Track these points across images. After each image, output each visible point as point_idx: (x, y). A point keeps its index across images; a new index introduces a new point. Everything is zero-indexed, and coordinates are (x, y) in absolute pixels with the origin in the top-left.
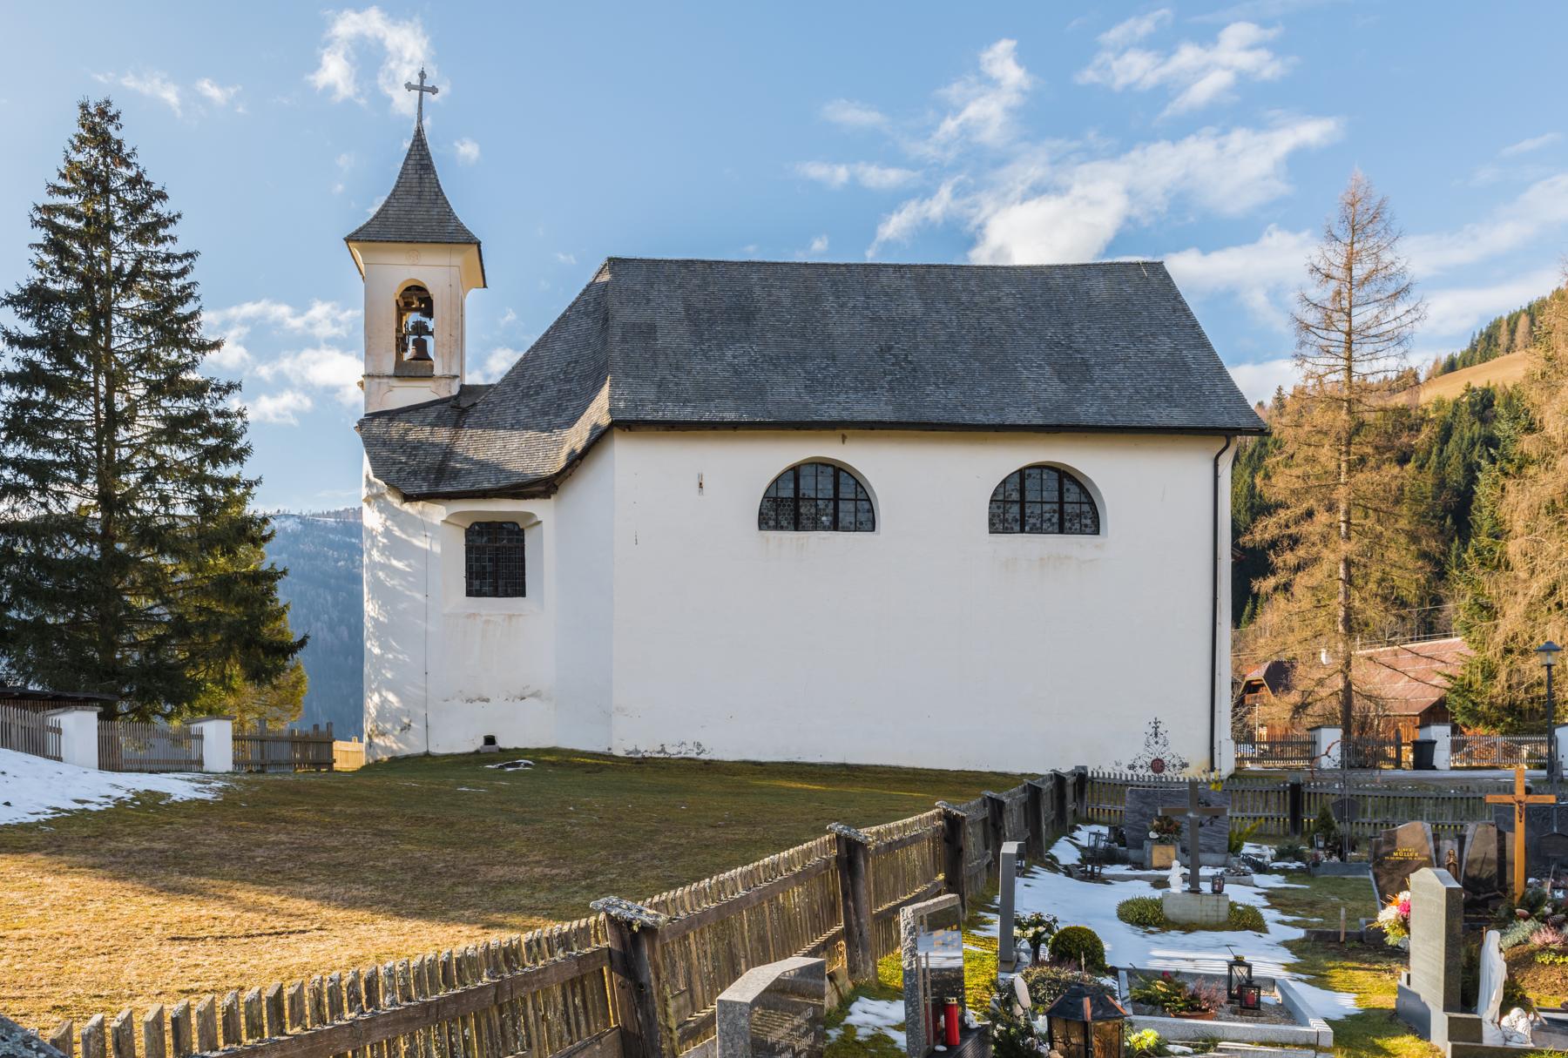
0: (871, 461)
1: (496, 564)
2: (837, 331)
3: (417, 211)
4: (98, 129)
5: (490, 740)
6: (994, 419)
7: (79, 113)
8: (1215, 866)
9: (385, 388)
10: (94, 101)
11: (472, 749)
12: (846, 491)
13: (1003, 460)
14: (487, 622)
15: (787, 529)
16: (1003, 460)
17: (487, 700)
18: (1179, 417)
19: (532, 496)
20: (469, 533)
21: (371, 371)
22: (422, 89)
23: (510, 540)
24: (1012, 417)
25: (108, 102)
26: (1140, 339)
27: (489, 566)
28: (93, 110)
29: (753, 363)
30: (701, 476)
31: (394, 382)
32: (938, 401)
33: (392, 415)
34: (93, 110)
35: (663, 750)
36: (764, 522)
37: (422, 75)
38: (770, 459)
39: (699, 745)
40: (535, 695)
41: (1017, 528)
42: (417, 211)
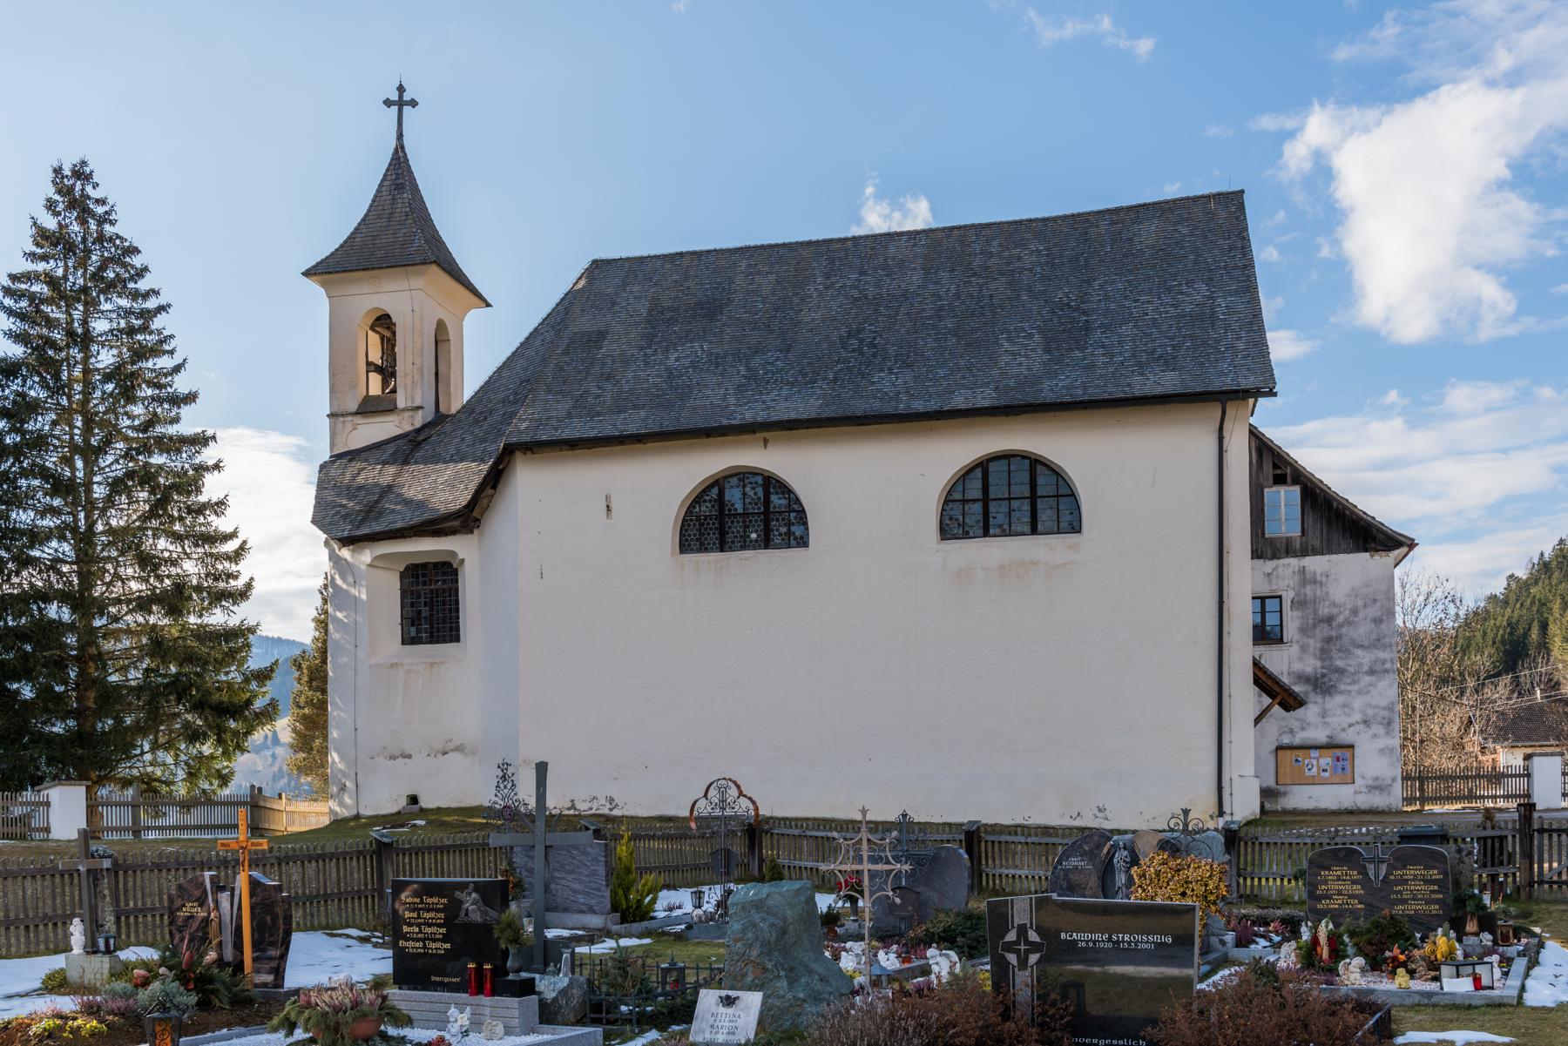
0: (798, 465)
1: (431, 609)
2: (806, 317)
3: (395, 236)
4: (73, 189)
5: (414, 800)
6: (934, 405)
7: (51, 175)
8: (640, 937)
9: (349, 426)
11: (394, 810)
12: (1045, 484)
13: (950, 454)
14: (409, 671)
15: (712, 550)
16: (950, 454)
17: (409, 757)
18: (1168, 382)
19: (453, 532)
20: (403, 576)
21: (336, 409)
22: (401, 103)
23: (444, 582)
24: (959, 401)
25: (83, 163)
26: (1169, 290)
27: (425, 612)
28: (67, 172)
29: (694, 365)
31: (358, 420)
32: (889, 386)
33: (352, 455)
34: (67, 172)
35: (573, 807)
36: (685, 546)
37: (401, 89)
38: (681, 474)
39: (612, 800)
40: (457, 749)
41: (1027, 529)
42: (395, 236)
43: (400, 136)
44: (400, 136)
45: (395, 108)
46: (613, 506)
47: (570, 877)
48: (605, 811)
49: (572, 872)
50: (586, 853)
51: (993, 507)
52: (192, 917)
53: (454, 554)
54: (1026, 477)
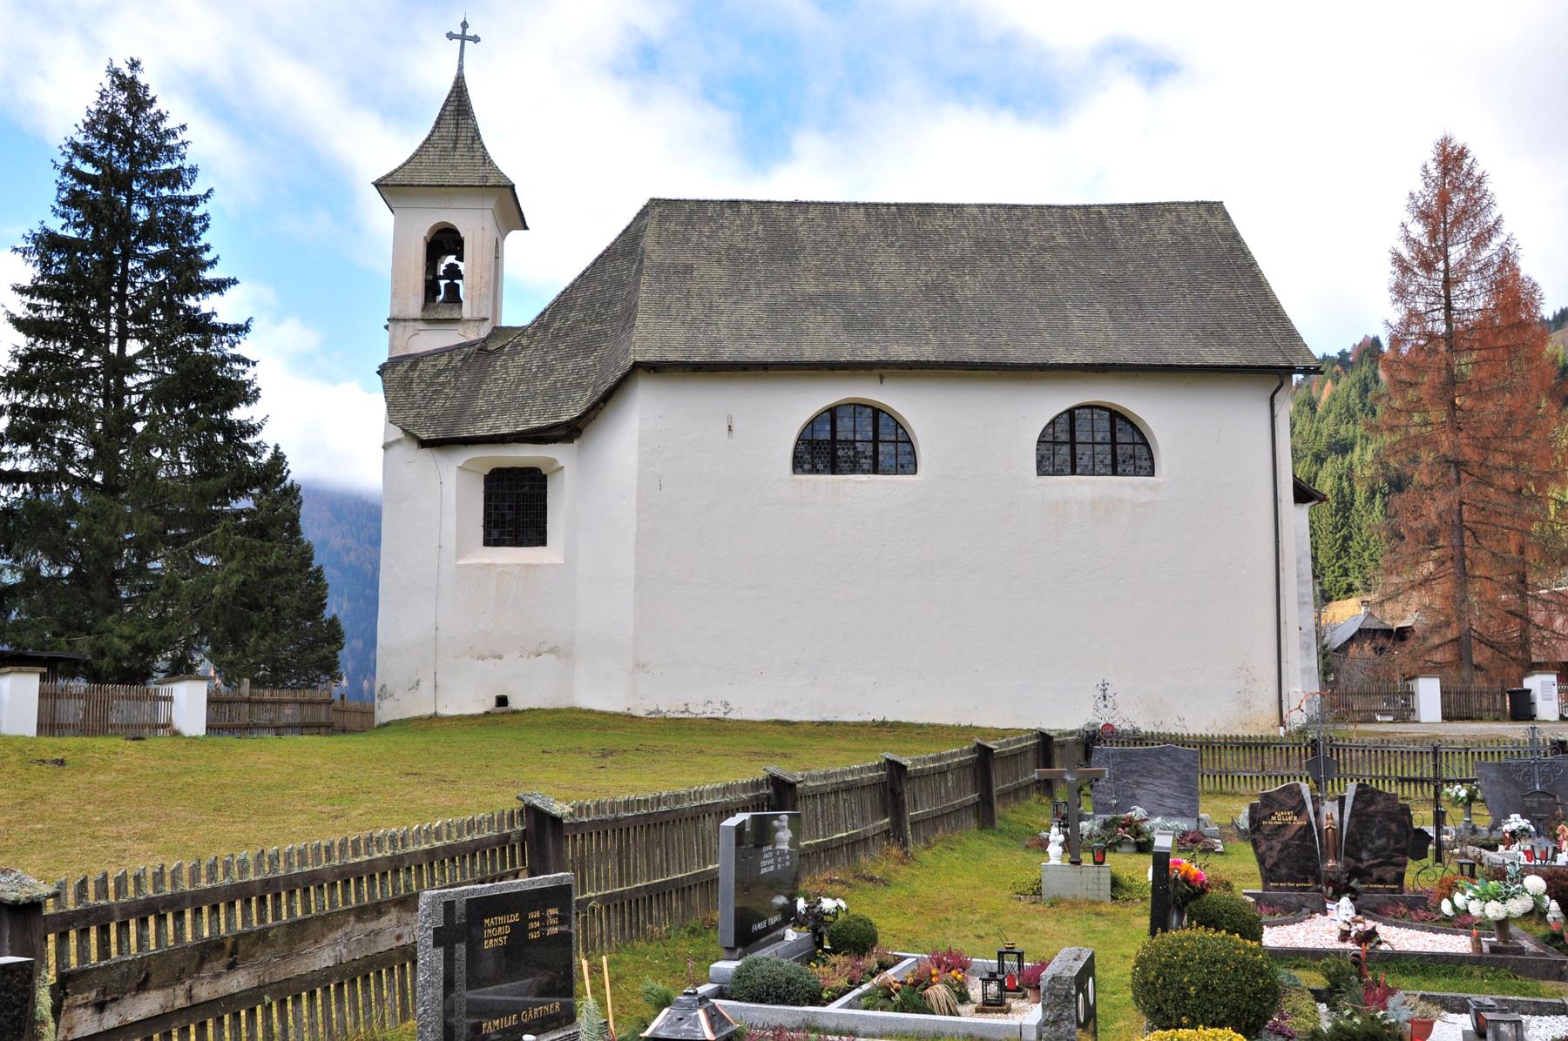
5: (502, 701)
10: (1458, 141)
12: (886, 433)
16: (802, 404)
17: (500, 657)
22: (463, 38)
23: (531, 487)
30: (730, 418)
31: (420, 325)
43: (461, 68)
44: (461, 68)
45: (458, 42)
46: (734, 427)
47: (1158, 782)
48: (720, 715)
49: (1161, 777)
50: (1177, 760)
51: (1079, 449)
52: (1285, 826)
53: (554, 461)
54: (1107, 425)
